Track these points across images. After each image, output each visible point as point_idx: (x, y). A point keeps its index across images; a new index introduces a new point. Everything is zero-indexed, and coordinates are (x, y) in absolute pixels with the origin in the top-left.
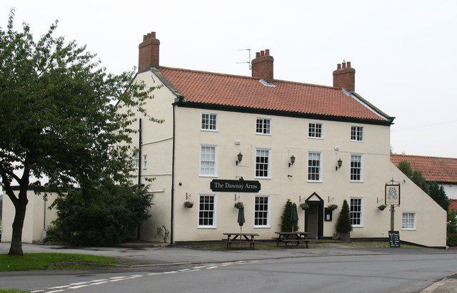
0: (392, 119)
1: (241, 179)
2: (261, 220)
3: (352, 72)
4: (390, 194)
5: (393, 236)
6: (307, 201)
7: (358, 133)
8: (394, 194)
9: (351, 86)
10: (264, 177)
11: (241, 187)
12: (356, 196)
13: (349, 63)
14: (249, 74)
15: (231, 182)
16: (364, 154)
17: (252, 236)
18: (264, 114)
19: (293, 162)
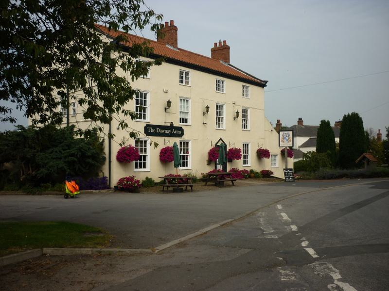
0: (266, 82)
1: (172, 124)
2: (140, 164)
3: (228, 48)
4: (284, 138)
5: (288, 173)
6: (216, 145)
7: (182, 78)
8: (287, 138)
9: (227, 59)
10: (185, 124)
11: (168, 132)
12: (246, 141)
13: (225, 42)
14: (210, 56)
15: (161, 127)
16: (249, 108)
17: (332, 167)
18: (247, 83)
19: (169, 106)
